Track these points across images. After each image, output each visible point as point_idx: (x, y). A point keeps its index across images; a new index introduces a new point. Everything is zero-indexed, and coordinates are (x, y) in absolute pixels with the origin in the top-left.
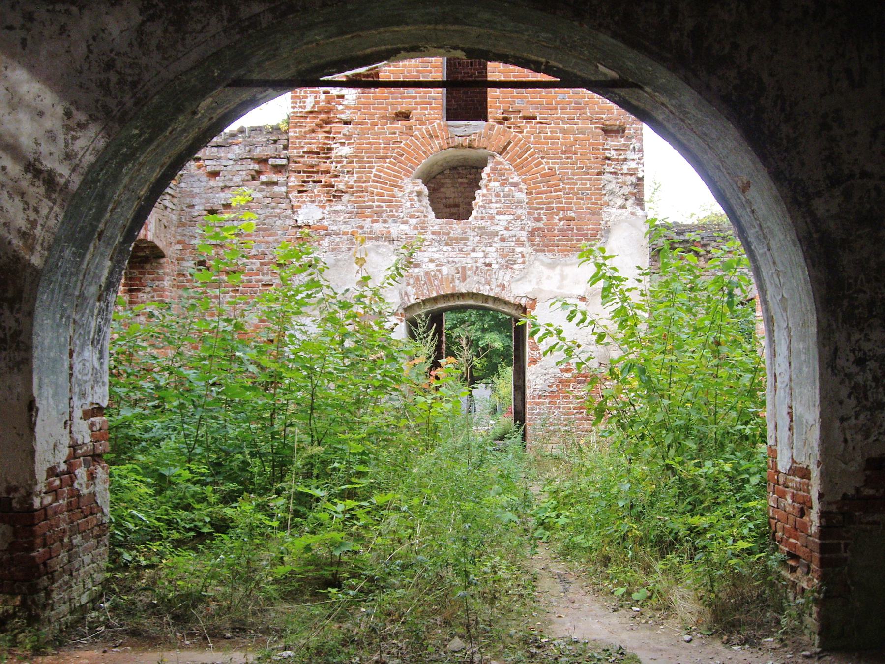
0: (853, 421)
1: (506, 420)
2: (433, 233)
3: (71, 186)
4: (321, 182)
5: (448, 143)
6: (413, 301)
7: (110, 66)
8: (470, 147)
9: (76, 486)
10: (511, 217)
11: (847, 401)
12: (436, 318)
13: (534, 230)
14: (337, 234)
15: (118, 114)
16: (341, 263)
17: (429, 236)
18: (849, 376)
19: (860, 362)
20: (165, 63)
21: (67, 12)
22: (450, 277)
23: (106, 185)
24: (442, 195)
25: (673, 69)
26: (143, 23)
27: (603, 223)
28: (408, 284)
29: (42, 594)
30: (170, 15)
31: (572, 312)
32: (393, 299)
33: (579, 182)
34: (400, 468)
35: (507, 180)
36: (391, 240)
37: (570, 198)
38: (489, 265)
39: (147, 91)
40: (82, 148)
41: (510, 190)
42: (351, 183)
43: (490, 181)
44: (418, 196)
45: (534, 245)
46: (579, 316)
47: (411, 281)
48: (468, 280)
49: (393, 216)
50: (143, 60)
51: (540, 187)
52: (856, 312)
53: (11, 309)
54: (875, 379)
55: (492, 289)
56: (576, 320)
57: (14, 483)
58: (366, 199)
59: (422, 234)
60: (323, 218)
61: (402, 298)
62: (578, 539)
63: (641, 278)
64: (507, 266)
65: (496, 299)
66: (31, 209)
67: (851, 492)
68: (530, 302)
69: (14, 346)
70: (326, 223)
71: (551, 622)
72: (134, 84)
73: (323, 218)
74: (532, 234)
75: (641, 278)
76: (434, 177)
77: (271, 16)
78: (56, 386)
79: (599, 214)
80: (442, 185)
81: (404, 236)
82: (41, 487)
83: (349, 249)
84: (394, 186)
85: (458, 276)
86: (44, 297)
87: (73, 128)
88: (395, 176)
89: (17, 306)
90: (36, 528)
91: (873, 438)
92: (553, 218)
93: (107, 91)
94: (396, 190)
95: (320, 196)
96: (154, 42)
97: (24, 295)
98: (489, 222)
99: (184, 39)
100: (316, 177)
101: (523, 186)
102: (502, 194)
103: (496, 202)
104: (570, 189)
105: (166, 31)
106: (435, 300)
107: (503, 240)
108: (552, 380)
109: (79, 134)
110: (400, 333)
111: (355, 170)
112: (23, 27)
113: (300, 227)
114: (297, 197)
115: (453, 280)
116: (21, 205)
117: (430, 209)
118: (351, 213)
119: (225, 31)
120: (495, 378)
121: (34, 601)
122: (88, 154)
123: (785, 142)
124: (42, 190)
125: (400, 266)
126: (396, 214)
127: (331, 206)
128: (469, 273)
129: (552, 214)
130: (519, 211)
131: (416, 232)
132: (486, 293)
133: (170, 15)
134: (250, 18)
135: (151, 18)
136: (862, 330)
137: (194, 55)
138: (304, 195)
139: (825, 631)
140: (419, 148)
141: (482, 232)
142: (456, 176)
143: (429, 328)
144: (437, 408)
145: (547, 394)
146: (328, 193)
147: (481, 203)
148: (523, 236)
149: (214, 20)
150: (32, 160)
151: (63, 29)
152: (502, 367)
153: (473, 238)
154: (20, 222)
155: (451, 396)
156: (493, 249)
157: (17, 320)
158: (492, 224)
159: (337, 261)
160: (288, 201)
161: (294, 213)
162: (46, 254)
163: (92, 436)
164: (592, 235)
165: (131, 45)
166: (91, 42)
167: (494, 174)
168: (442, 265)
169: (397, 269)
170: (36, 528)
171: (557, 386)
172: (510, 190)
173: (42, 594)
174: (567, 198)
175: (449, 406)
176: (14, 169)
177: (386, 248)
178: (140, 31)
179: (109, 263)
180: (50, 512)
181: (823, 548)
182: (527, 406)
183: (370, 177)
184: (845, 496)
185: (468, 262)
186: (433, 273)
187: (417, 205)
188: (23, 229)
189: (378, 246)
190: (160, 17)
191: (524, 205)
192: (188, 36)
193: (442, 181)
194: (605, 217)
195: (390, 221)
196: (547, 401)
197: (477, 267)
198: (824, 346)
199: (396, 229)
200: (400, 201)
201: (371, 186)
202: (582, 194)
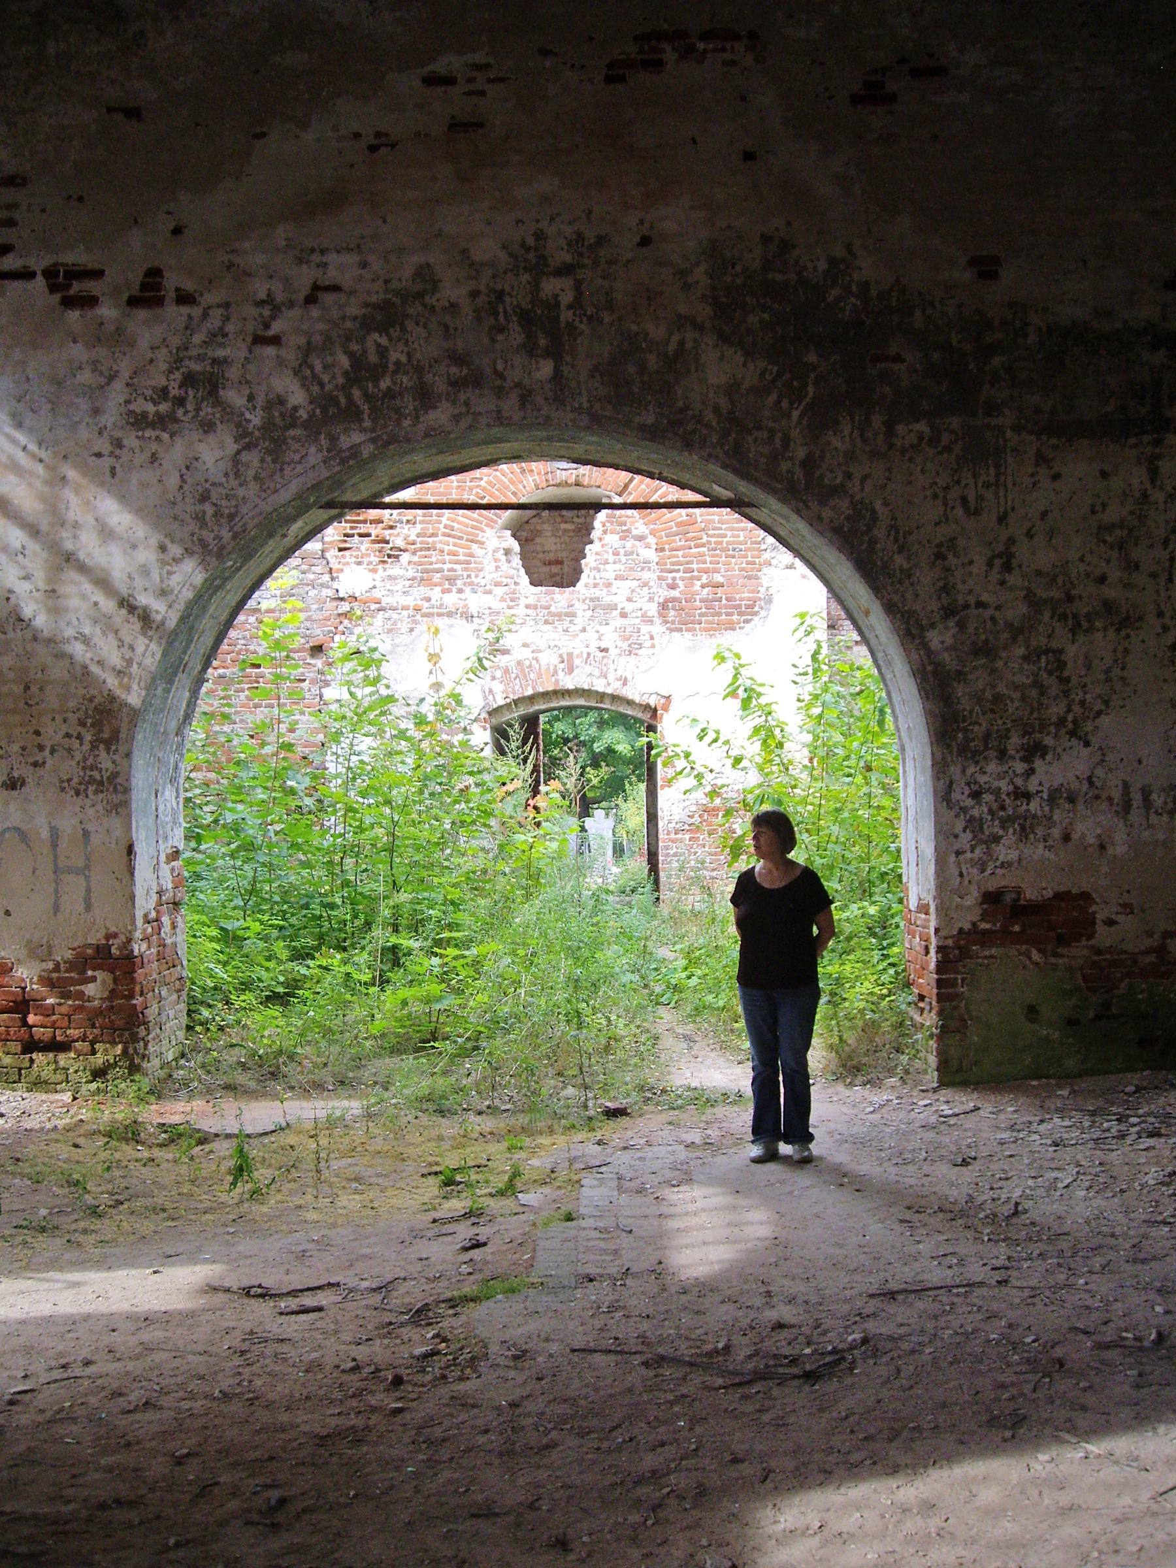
0: (969, 855)
1: (638, 865)
2: (528, 607)
3: (168, 622)
4: (368, 535)
5: (547, 481)
6: (501, 702)
7: (204, 498)
8: (577, 484)
9: (163, 935)
10: (636, 583)
11: (962, 835)
12: (530, 723)
13: (667, 601)
14: (395, 609)
15: (215, 549)
16: (400, 649)
17: (521, 611)
18: (964, 810)
19: (976, 795)
20: (264, 495)
21: (158, 438)
22: (552, 668)
23: (197, 617)
24: (539, 548)
25: (783, 500)
26: (239, 452)
27: (762, 590)
28: (493, 678)
29: (142, 1043)
30: (267, 443)
31: (703, 730)
32: (475, 699)
33: (729, 533)
34: (496, 922)
35: (629, 531)
36: (469, 617)
37: (717, 556)
38: (605, 650)
39: (244, 525)
40: (178, 583)
41: (634, 546)
42: (413, 537)
43: (605, 532)
44: (506, 554)
45: (667, 622)
46: (711, 736)
47: (498, 674)
48: (576, 671)
49: (471, 584)
50: (241, 492)
51: (674, 541)
52: (972, 744)
53: (108, 750)
54: (990, 811)
55: (609, 684)
56: (708, 739)
57: (113, 929)
58: (434, 559)
59: (509, 607)
60: (375, 587)
61: (485, 698)
62: (710, 998)
63: (798, 679)
64: (630, 652)
65: (615, 698)
66: (126, 646)
67: (967, 926)
68: (663, 701)
69: (111, 789)
70: (377, 594)
71: (669, 1073)
72: (231, 517)
73: (375, 587)
74: (664, 606)
75: (798, 679)
76: (527, 522)
77: (372, 447)
78: (148, 829)
79: (757, 578)
80: (538, 533)
81: (487, 612)
82: (138, 934)
83: (412, 630)
84: (472, 541)
85: (562, 666)
86: (141, 737)
87: (168, 562)
88: (473, 527)
89: (113, 748)
90: (136, 975)
91: (989, 872)
92: (692, 585)
93: (203, 524)
94: (475, 546)
95: (369, 555)
96: (251, 473)
97: (121, 735)
98: (605, 590)
99: (282, 470)
100: (363, 529)
101: (652, 540)
102: (622, 551)
103: (614, 563)
104: (716, 543)
105: (262, 460)
106: (531, 699)
107: (624, 615)
108: (693, 808)
109: (175, 569)
110: (482, 736)
111: (418, 519)
112: (112, 454)
113: (342, 599)
114: (337, 557)
115: (555, 672)
116: (116, 643)
117: (523, 571)
118: (413, 579)
119: (325, 462)
120: (620, 801)
121: (135, 1049)
122: (184, 590)
123: (898, 572)
124: (138, 625)
125: (481, 655)
126: (476, 581)
127: (385, 570)
128: (577, 662)
129: (692, 578)
130: (646, 575)
131: (504, 605)
132: (601, 689)
133: (267, 443)
134: (351, 448)
135: (248, 447)
136: (977, 763)
137: (294, 487)
138: (347, 553)
139: (944, 1066)
140: (507, 488)
141: (596, 605)
142: (558, 520)
143: (524, 742)
144: (540, 847)
145: (686, 827)
146: (380, 551)
147: (593, 565)
148: (653, 609)
149: (313, 450)
150: (126, 596)
151: (154, 458)
152: (631, 784)
153: (583, 614)
154: (115, 659)
155: (556, 833)
156: (610, 628)
157: (114, 762)
158: (609, 593)
159: (395, 646)
160: (325, 562)
161: (333, 579)
162: (144, 693)
163: (173, 882)
164: (747, 607)
165: (226, 475)
166: (184, 471)
167: (612, 523)
168: (540, 651)
169: (480, 660)
170: (136, 975)
171: (700, 816)
172: (634, 546)
173: (142, 1043)
174: (712, 556)
175: (554, 846)
176: (108, 605)
177: (463, 629)
178: (235, 460)
179: (187, 694)
180: (145, 960)
181: (940, 983)
182: (660, 844)
183: (439, 529)
184: (961, 930)
185: (576, 646)
186: (527, 663)
187: (504, 566)
188: (118, 667)
189: (451, 626)
190: (256, 446)
191: (653, 566)
192: (285, 466)
193: (538, 528)
194: (765, 581)
195: (468, 590)
196: (687, 837)
197: (589, 654)
198: (939, 779)
199: (476, 602)
200: (480, 563)
201: (440, 542)
202: (734, 550)
